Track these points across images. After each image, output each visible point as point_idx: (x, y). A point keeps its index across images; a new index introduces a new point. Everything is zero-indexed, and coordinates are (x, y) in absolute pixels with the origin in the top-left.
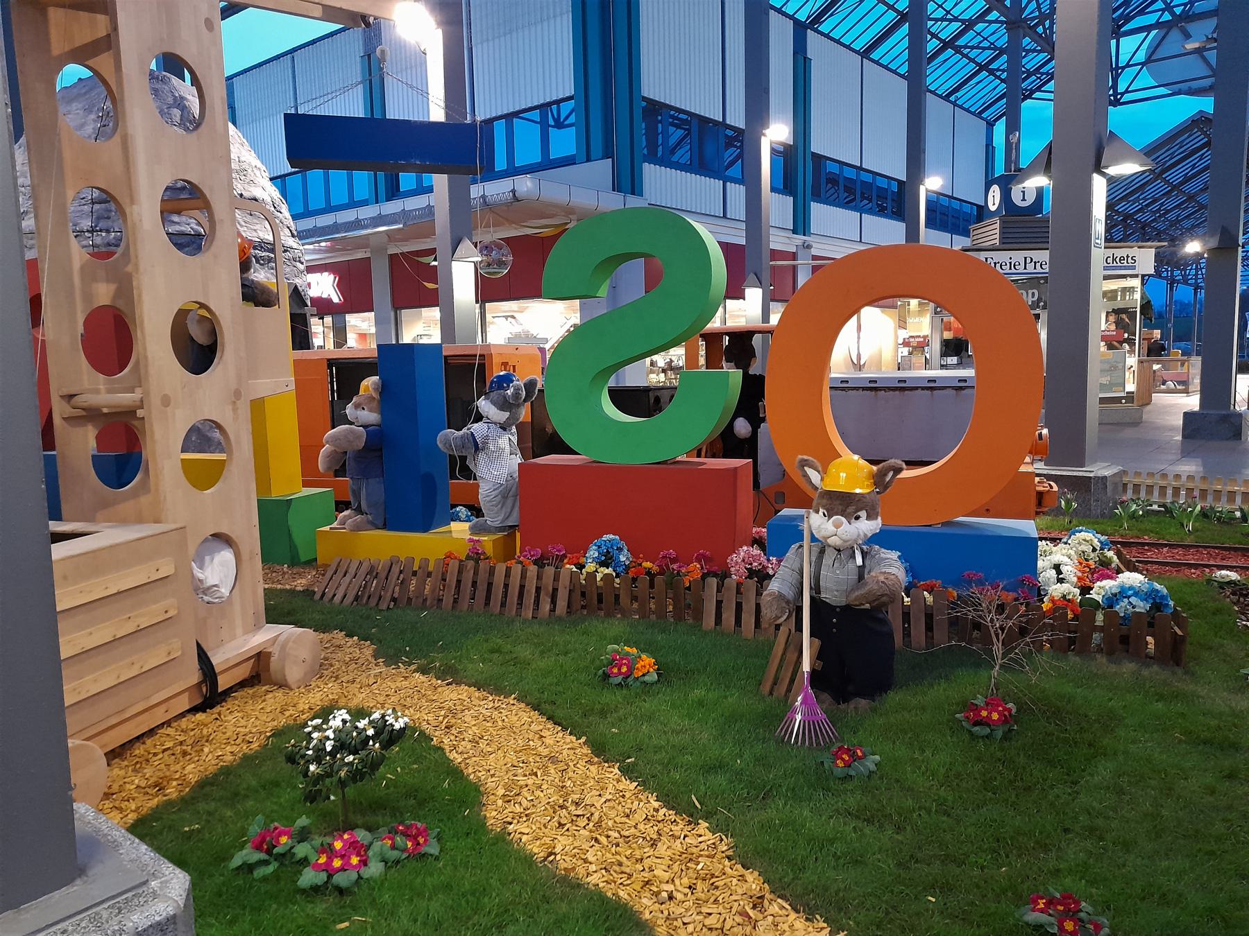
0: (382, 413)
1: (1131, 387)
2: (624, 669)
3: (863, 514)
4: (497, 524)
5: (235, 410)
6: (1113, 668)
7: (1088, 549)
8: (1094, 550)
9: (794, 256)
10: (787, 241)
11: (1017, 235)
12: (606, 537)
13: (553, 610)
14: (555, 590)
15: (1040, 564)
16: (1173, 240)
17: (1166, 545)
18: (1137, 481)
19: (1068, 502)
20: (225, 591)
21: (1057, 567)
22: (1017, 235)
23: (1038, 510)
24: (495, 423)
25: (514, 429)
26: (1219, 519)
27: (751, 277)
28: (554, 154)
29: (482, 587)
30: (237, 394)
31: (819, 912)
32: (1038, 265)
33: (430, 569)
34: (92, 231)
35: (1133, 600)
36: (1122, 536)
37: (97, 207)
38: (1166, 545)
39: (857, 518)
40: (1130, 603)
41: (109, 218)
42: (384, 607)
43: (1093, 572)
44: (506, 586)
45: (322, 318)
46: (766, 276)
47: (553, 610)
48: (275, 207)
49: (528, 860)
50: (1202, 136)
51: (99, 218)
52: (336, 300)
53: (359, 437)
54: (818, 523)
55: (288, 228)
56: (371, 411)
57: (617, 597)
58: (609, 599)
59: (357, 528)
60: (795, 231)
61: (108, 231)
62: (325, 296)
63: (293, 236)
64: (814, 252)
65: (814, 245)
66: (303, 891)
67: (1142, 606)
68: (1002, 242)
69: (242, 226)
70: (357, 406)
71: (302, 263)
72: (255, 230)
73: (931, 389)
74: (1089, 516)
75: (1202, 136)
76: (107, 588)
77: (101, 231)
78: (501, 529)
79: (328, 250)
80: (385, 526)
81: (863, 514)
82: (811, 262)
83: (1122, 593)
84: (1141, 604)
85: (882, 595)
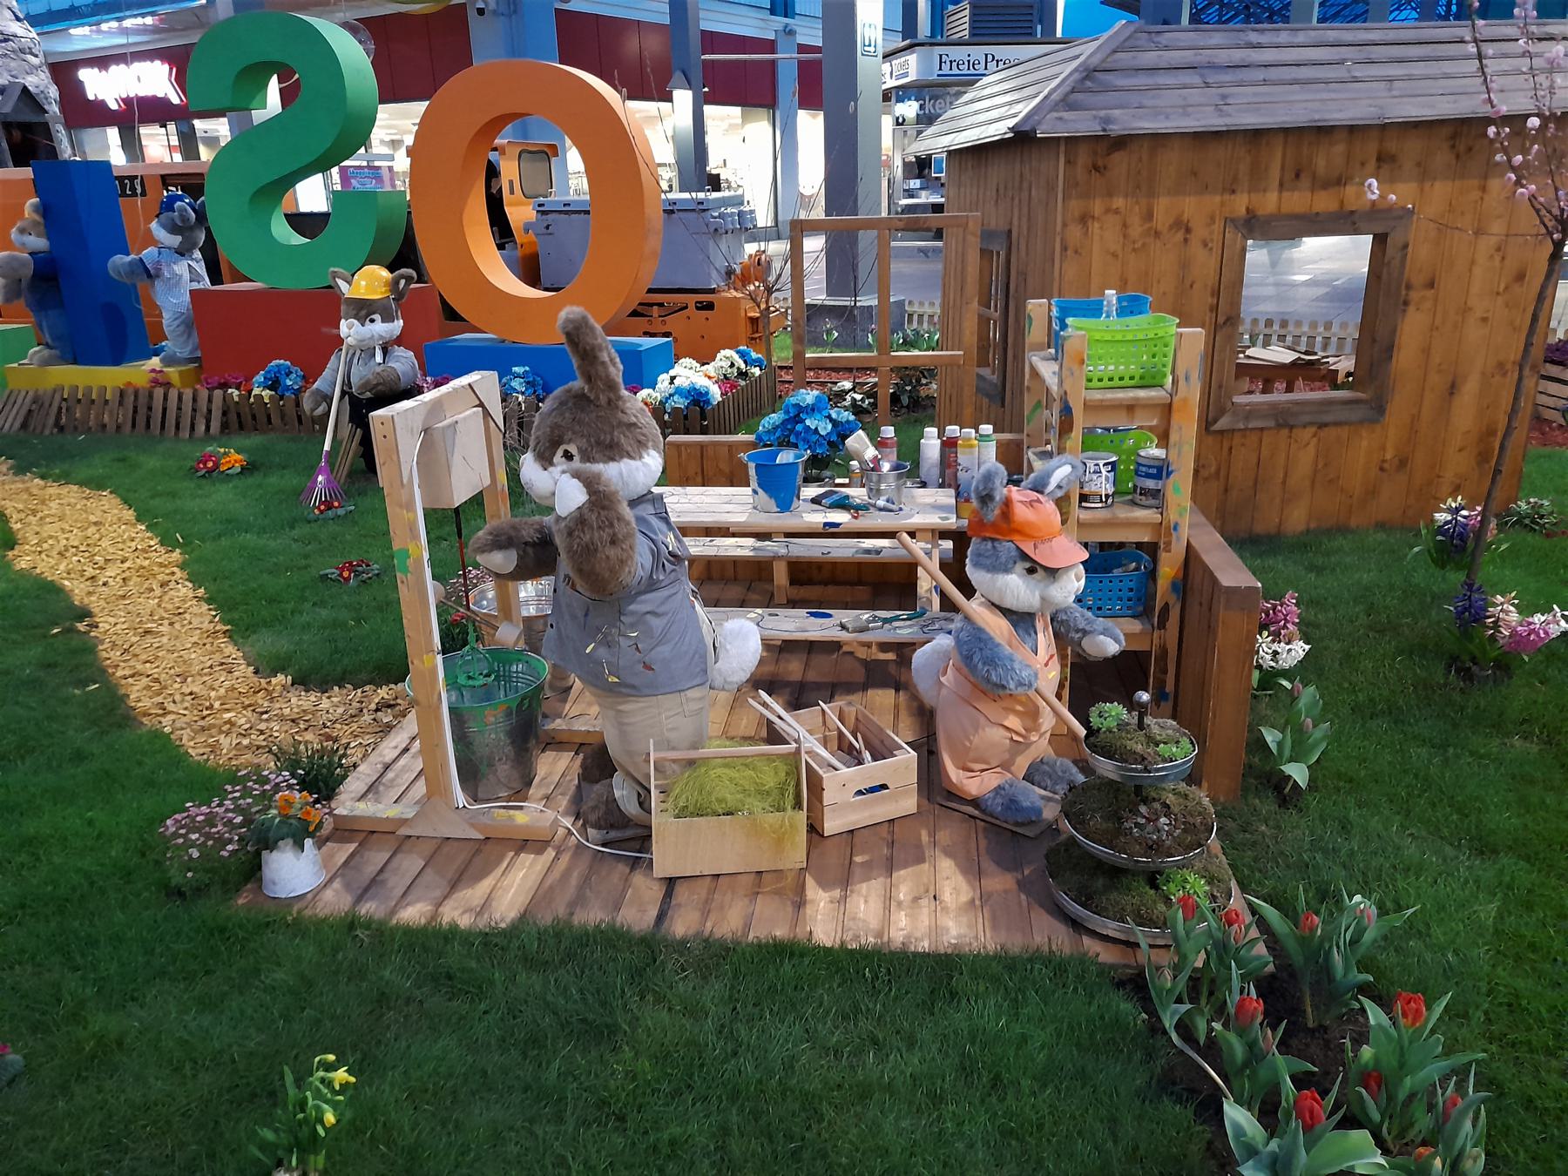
0: (48, 239)
2: (210, 464)
3: (377, 317)
4: (186, 355)
9: (770, 46)
10: (762, 24)
11: (1010, 25)
12: (274, 363)
13: (208, 428)
14: (210, 411)
18: (920, 311)
22: (1010, 25)
24: (169, 248)
25: (197, 254)
27: (678, 76)
29: (142, 411)
32: (954, 64)
33: (94, 397)
39: (372, 321)
42: (47, 432)
44: (165, 410)
45: (165, 126)
46: (697, 74)
47: (208, 428)
49: (925, 955)
52: (175, 100)
53: (23, 263)
54: (349, 329)
56: (38, 236)
57: (269, 417)
58: (262, 418)
59: (47, 362)
60: (773, 12)
62: (161, 95)
63: (18, 19)
64: (801, 40)
65: (798, 30)
68: (972, 35)
70: (22, 231)
71: (36, 56)
73: (566, 212)
78: (191, 360)
79: (154, 30)
80: (75, 362)
81: (377, 317)
82: (796, 55)
85: (378, 384)
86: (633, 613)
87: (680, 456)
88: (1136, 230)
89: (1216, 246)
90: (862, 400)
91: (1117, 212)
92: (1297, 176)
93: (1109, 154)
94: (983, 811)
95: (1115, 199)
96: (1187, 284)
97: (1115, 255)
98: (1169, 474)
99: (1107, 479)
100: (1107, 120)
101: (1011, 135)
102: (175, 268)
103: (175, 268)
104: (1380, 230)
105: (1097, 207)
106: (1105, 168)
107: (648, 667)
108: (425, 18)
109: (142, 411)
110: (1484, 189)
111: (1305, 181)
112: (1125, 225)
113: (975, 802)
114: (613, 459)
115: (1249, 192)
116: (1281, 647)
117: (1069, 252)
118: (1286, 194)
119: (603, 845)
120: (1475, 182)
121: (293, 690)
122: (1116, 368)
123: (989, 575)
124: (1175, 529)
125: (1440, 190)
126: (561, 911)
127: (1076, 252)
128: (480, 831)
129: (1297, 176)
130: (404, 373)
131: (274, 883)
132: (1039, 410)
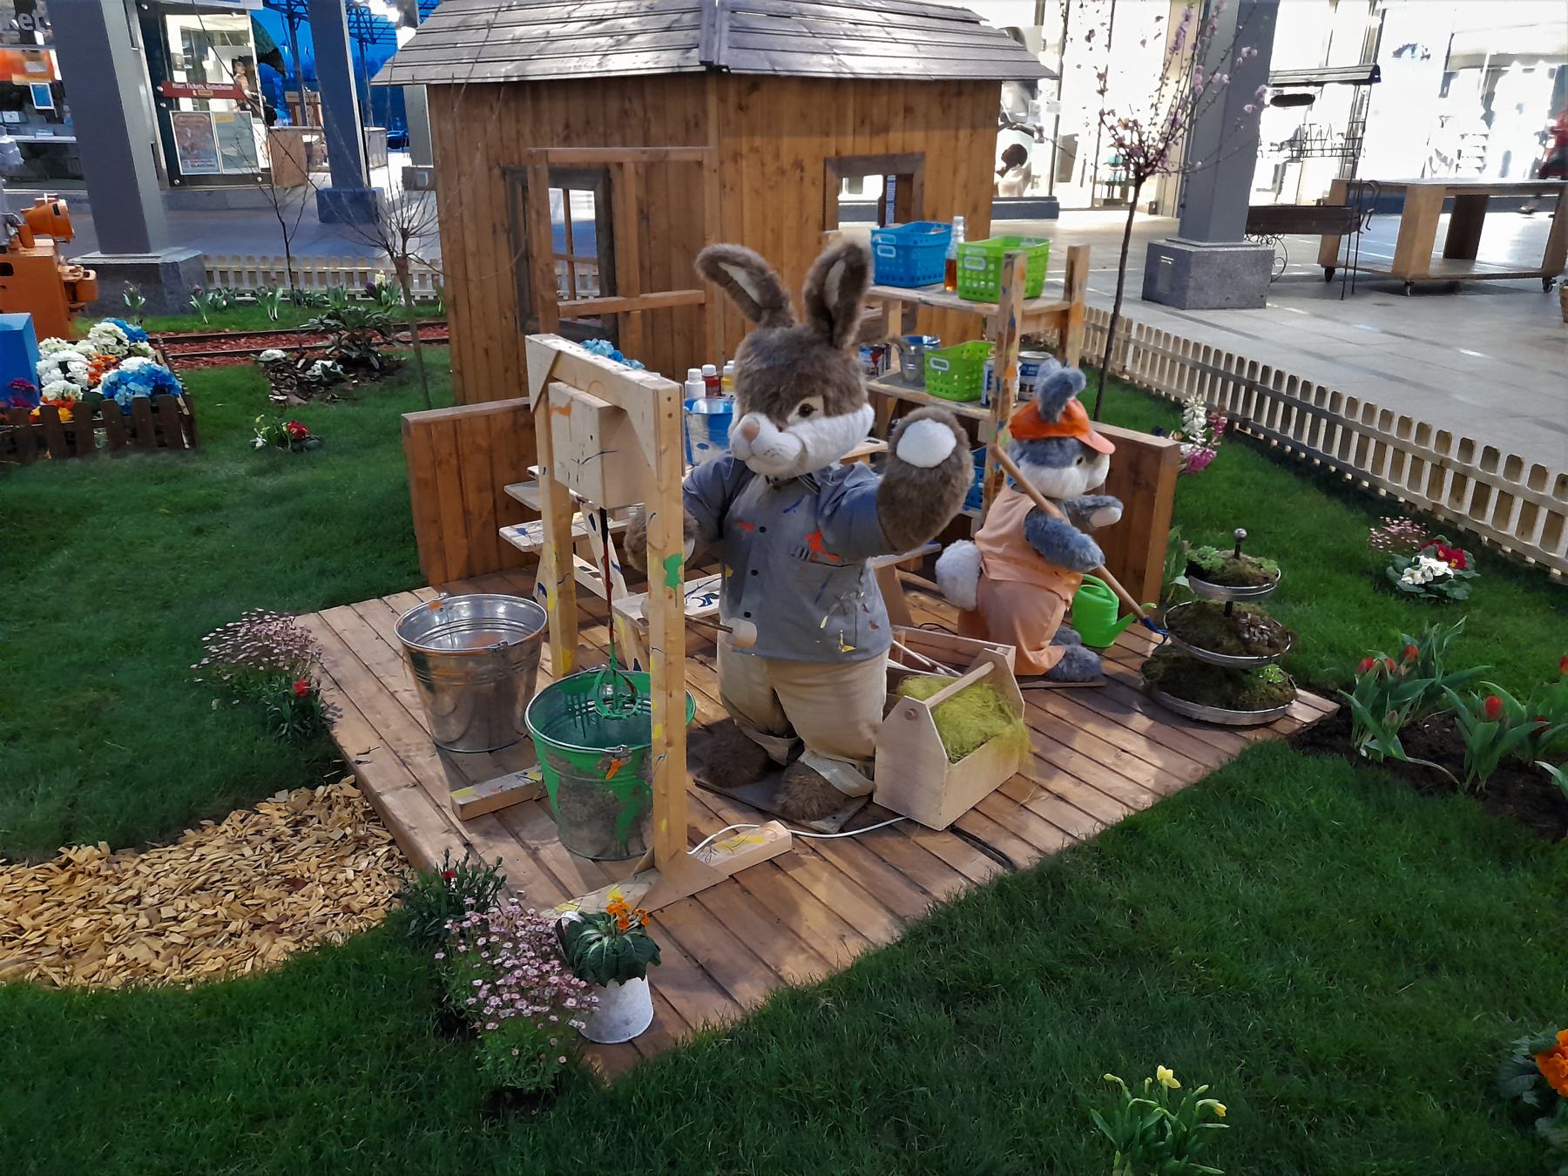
1: (263, 163)
6: (116, 462)
7: (112, 341)
8: (119, 342)
15: (40, 365)
16: (1429, 540)
17: (243, 336)
19: (133, 297)
21: (63, 366)
23: (73, 306)
26: (309, 304)
28: (1056, 344)
35: (132, 385)
36: (201, 331)
38: (243, 336)
40: (128, 390)
43: (97, 367)
66: (1408, 596)
67: (142, 391)
74: (165, 313)
83: (123, 379)
84: (141, 388)
87: (430, 434)
88: (771, 168)
89: (820, 183)
90: (334, 366)
92: (863, 122)
93: (749, 94)
94: (1057, 680)
96: (804, 219)
100: (772, 63)
101: (703, 68)
104: (545, 174)
110: (957, 138)
111: (867, 129)
112: (763, 164)
113: (1047, 676)
115: (871, 136)
118: (858, 139)
119: (841, 831)
120: (952, 132)
121: (118, 857)
122: (987, 284)
123: (1056, 471)
125: (937, 136)
129: (863, 122)
131: (627, 1023)
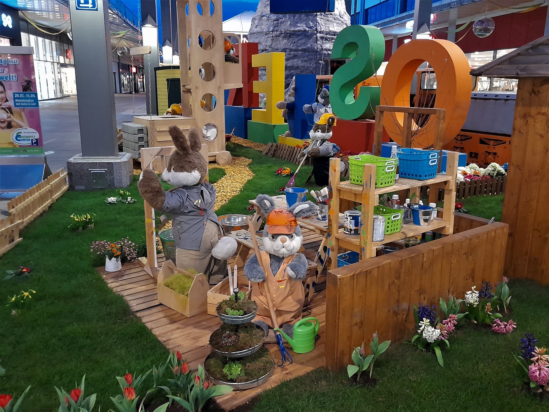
5: (219, 92)
20: (212, 139)
29: (291, 154)
30: (220, 87)
31: (89, 252)
34: (272, 31)
37: (275, 22)
39: (318, 131)
41: (278, 26)
48: (340, 16)
50: (58, 9)
51: (275, 27)
55: (346, 24)
59: (288, 135)
61: (277, 31)
69: (323, 26)
72: (328, 27)
75: (58, 9)
76: (450, 167)
77: (275, 31)
86: (178, 220)
91: (543, 114)
93: (541, 86)
95: (543, 108)
97: (541, 136)
98: (361, 225)
99: (350, 222)
102: (321, 110)
103: (321, 110)
105: (533, 111)
106: (539, 92)
107: (180, 238)
108: (529, 13)
109: (291, 154)
114: (182, 171)
116: (431, 329)
117: (516, 132)
124: (363, 250)
126: (125, 293)
127: (520, 132)
128: (153, 275)
130: (322, 151)
132: (414, 197)
